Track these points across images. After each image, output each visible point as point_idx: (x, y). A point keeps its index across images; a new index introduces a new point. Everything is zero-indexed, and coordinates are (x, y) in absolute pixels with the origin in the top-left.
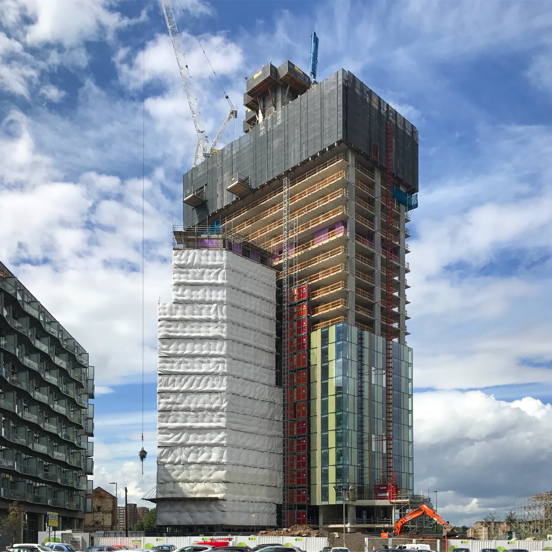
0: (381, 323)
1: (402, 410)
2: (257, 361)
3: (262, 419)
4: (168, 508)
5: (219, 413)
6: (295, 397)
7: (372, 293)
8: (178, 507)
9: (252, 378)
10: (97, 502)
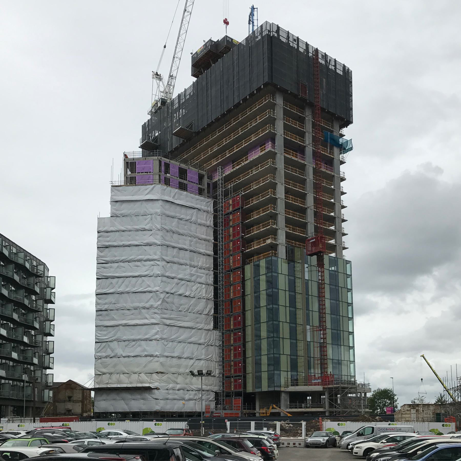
0: (315, 225)
1: (341, 303)
2: (193, 263)
3: (200, 315)
4: (104, 396)
5: (153, 311)
6: (232, 294)
7: (305, 199)
8: (113, 395)
9: (187, 277)
10: (68, 393)
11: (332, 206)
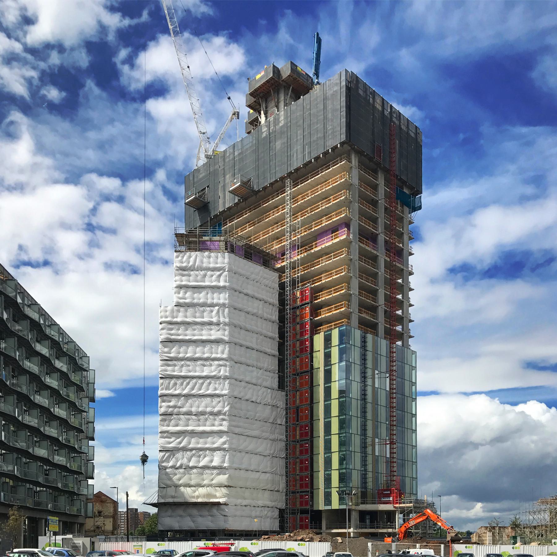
0: (385, 326)
2: (259, 364)
3: (264, 423)
4: (169, 512)
5: (221, 417)
6: (298, 401)
8: (180, 511)
9: (254, 381)
11: (400, 304)
